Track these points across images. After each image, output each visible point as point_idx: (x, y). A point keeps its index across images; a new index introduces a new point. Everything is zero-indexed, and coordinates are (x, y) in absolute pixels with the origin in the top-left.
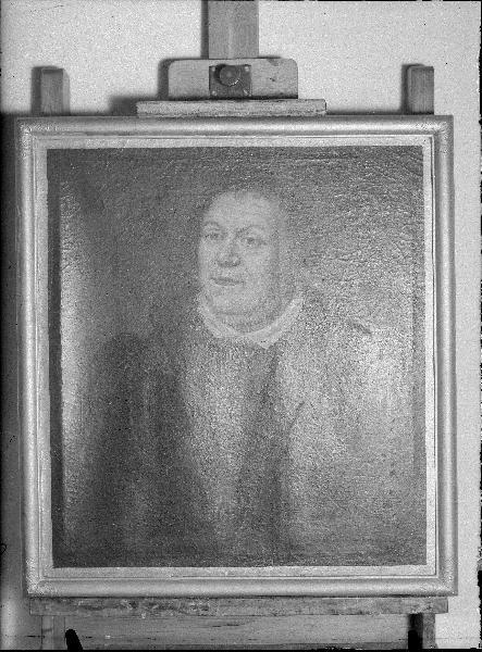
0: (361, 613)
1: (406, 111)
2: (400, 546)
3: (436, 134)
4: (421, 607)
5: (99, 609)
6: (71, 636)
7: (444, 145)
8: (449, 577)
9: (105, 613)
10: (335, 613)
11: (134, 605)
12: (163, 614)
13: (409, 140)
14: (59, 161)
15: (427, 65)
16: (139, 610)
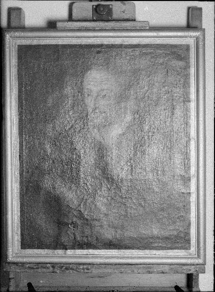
0: (163, 273)
1: (189, 27)
2: (181, 241)
3: (197, 38)
4: (192, 270)
5: (38, 268)
6: (30, 285)
7: (199, 44)
8: (202, 256)
9: (39, 270)
10: (149, 272)
11: (53, 267)
12: (67, 271)
13: (183, 42)
14: (24, 51)
15: (199, 7)
16: (56, 270)
